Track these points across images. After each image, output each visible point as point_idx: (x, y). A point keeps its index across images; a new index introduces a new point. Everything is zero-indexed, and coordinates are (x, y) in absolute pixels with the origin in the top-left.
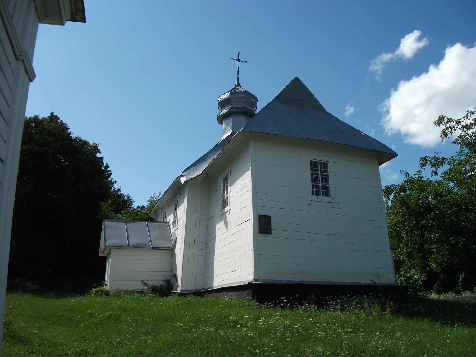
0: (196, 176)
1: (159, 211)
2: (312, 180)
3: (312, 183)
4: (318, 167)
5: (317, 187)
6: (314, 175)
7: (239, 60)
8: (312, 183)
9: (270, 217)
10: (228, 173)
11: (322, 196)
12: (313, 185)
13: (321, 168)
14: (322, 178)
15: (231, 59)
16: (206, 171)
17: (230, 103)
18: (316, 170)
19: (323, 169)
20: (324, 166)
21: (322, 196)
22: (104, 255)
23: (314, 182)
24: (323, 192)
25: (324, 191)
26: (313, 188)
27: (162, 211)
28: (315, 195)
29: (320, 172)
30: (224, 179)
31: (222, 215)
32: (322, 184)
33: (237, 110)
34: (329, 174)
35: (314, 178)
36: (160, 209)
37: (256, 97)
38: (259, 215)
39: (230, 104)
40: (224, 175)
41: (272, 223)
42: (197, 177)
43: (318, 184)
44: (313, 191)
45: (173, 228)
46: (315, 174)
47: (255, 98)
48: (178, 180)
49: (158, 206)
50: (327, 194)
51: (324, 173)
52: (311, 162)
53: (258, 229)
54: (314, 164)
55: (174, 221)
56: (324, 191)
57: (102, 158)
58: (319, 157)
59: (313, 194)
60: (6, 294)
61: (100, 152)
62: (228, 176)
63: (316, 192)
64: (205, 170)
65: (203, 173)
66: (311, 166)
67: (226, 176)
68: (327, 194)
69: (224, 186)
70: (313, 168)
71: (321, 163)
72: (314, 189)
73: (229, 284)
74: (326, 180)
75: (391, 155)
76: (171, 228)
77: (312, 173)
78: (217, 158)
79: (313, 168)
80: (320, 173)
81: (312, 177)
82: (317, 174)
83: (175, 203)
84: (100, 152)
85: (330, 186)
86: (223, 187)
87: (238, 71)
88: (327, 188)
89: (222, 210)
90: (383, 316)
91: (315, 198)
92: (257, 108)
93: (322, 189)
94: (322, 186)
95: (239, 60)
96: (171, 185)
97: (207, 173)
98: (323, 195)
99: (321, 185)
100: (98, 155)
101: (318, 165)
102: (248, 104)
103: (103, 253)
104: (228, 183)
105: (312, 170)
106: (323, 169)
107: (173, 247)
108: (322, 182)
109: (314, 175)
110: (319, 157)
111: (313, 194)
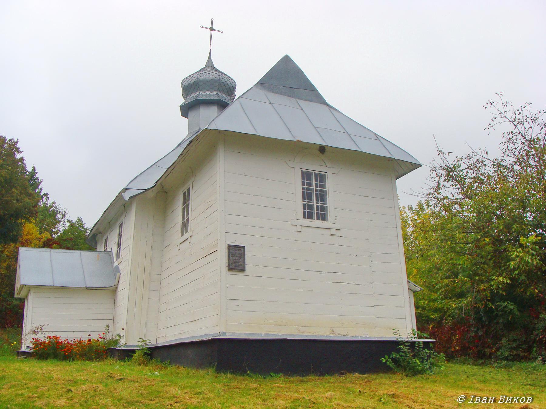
0: (147, 190)
1: (99, 236)
2: (304, 198)
3: (303, 201)
4: (312, 181)
5: (310, 207)
6: (306, 191)
7: (212, 29)
8: (303, 201)
9: (244, 247)
10: (189, 187)
11: (317, 219)
12: (304, 205)
13: (316, 181)
14: (317, 195)
15: (202, 27)
16: (161, 183)
17: (199, 88)
18: (310, 185)
19: (318, 183)
20: (321, 178)
21: (317, 219)
22: (22, 295)
23: (306, 200)
24: (318, 214)
25: (320, 212)
26: (304, 208)
27: (102, 237)
28: (308, 219)
29: (315, 187)
30: (184, 194)
31: (180, 244)
32: (316, 203)
33: (207, 99)
34: (327, 189)
35: (307, 195)
36: (100, 233)
37: (234, 81)
38: (228, 245)
39: (199, 89)
40: (184, 189)
41: (246, 256)
42: (148, 191)
43: (312, 202)
44: (304, 212)
45: (117, 260)
46: (308, 189)
47: (233, 82)
48: (119, 197)
49: (97, 229)
50: (323, 217)
51: (320, 188)
52: (303, 173)
53: (227, 264)
54: (306, 176)
55: (118, 251)
56: (320, 212)
57: (22, 160)
58: (315, 167)
59: (305, 217)
60: (327, 221)
61: (19, 152)
62: (188, 190)
63: (309, 216)
64: (159, 182)
65: (157, 185)
66: (303, 179)
67: (186, 190)
68: (323, 217)
69: (184, 203)
70: (305, 181)
71: (316, 175)
72: (307, 210)
73: (189, 337)
74: (322, 197)
75: (412, 165)
76: (114, 259)
77: (303, 189)
78: (174, 165)
79: (305, 181)
80: (314, 188)
81: (303, 193)
82: (310, 190)
83: (120, 226)
84: (19, 152)
85: (328, 206)
86: (183, 206)
87: (211, 45)
88: (323, 209)
89: (181, 237)
90: (19, 367)
91: (307, 222)
92: (235, 95)
93: (318, 210)
94: (317, 207)
95: (212, 29)
96: (113, 201)
97: (162, 185)
98: (318, 219)
99: (315, 204)
100: (18, 156)
101: (313, 178)
102: (223, 90)
103: (19, 294)
104: (189, 200)
105: (303, 184)
106: (318, 183)
107: (116, 287)
108: (317, 200)
109: (306, 191)
110: (315, 167)
111: (305, 217)
